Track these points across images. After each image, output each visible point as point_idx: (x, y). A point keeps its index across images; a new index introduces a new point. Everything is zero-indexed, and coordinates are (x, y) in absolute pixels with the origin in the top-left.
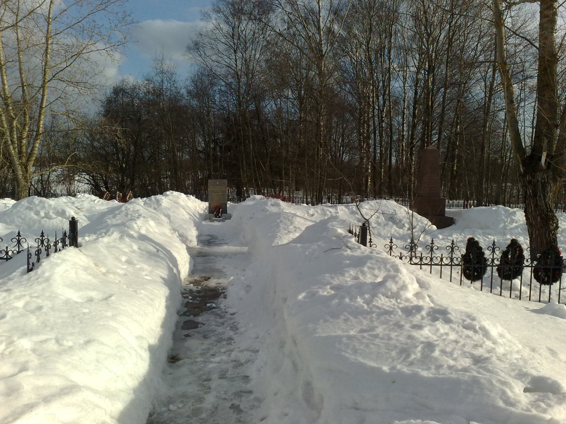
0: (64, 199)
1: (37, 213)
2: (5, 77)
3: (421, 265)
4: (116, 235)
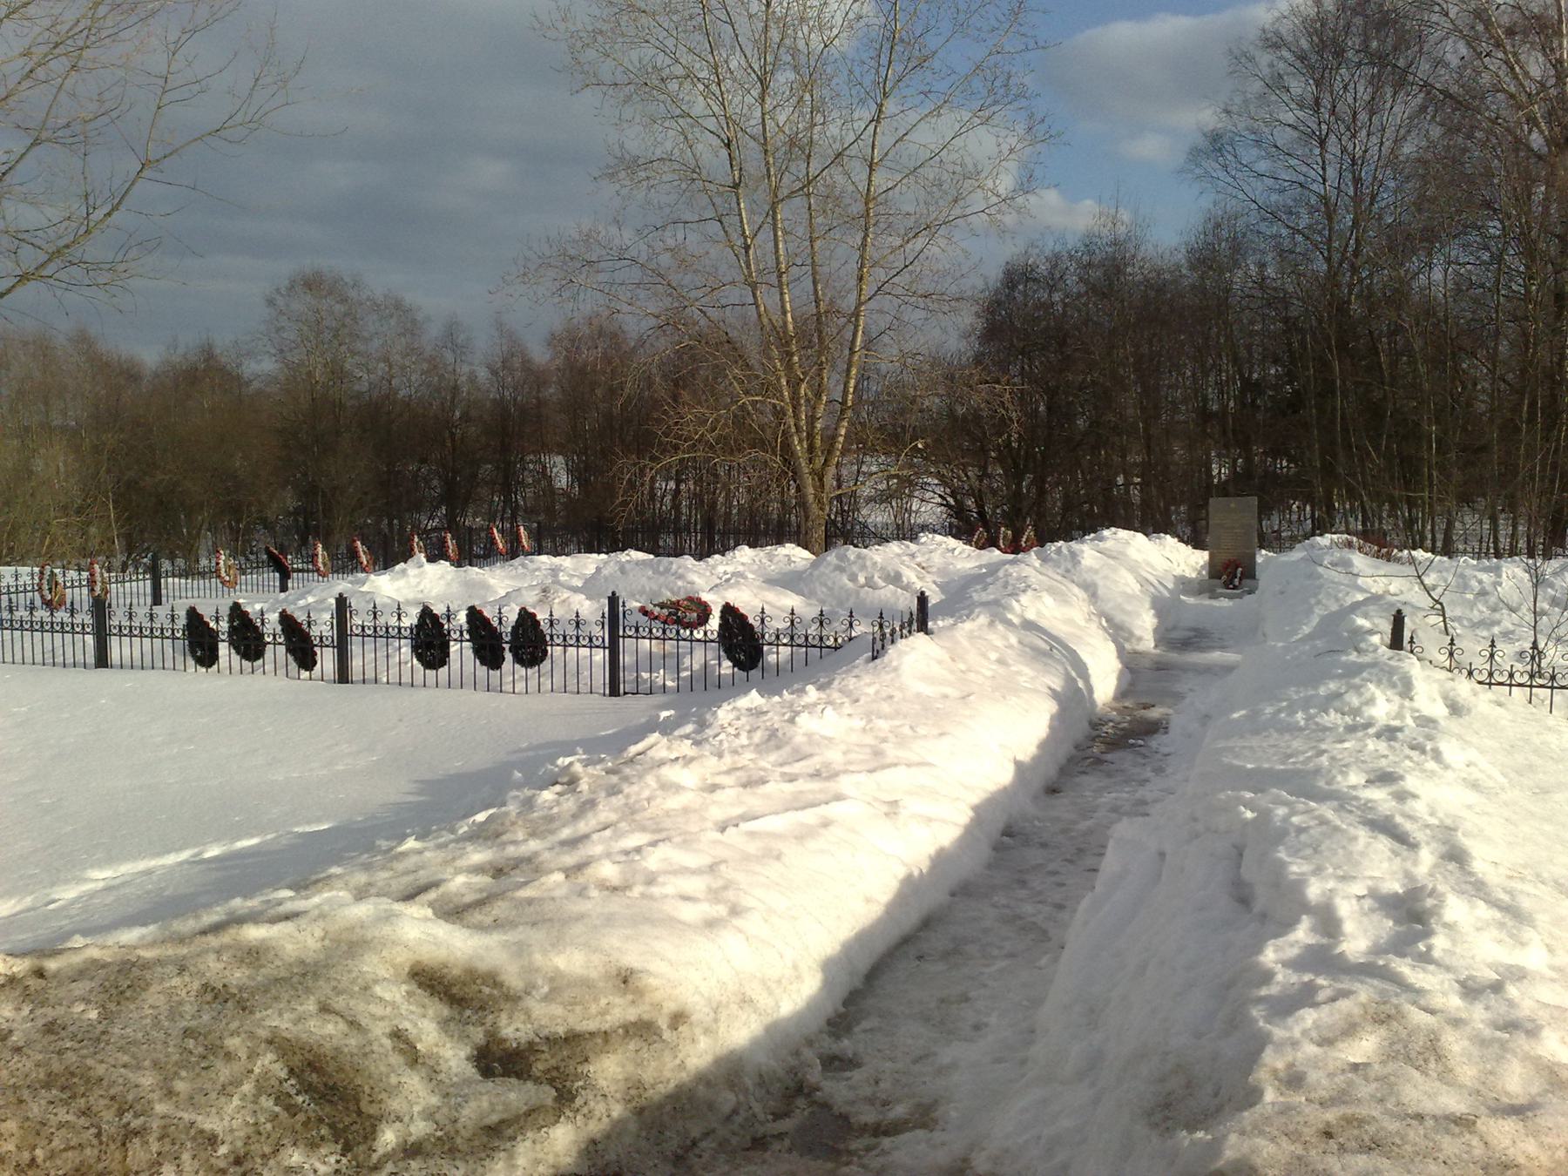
0: (894, 547)
1: (853, 578)
2: (787, 297)
3: (1511, 685)
4: (983, 619)
